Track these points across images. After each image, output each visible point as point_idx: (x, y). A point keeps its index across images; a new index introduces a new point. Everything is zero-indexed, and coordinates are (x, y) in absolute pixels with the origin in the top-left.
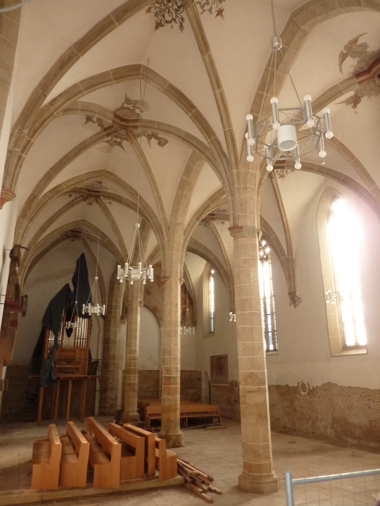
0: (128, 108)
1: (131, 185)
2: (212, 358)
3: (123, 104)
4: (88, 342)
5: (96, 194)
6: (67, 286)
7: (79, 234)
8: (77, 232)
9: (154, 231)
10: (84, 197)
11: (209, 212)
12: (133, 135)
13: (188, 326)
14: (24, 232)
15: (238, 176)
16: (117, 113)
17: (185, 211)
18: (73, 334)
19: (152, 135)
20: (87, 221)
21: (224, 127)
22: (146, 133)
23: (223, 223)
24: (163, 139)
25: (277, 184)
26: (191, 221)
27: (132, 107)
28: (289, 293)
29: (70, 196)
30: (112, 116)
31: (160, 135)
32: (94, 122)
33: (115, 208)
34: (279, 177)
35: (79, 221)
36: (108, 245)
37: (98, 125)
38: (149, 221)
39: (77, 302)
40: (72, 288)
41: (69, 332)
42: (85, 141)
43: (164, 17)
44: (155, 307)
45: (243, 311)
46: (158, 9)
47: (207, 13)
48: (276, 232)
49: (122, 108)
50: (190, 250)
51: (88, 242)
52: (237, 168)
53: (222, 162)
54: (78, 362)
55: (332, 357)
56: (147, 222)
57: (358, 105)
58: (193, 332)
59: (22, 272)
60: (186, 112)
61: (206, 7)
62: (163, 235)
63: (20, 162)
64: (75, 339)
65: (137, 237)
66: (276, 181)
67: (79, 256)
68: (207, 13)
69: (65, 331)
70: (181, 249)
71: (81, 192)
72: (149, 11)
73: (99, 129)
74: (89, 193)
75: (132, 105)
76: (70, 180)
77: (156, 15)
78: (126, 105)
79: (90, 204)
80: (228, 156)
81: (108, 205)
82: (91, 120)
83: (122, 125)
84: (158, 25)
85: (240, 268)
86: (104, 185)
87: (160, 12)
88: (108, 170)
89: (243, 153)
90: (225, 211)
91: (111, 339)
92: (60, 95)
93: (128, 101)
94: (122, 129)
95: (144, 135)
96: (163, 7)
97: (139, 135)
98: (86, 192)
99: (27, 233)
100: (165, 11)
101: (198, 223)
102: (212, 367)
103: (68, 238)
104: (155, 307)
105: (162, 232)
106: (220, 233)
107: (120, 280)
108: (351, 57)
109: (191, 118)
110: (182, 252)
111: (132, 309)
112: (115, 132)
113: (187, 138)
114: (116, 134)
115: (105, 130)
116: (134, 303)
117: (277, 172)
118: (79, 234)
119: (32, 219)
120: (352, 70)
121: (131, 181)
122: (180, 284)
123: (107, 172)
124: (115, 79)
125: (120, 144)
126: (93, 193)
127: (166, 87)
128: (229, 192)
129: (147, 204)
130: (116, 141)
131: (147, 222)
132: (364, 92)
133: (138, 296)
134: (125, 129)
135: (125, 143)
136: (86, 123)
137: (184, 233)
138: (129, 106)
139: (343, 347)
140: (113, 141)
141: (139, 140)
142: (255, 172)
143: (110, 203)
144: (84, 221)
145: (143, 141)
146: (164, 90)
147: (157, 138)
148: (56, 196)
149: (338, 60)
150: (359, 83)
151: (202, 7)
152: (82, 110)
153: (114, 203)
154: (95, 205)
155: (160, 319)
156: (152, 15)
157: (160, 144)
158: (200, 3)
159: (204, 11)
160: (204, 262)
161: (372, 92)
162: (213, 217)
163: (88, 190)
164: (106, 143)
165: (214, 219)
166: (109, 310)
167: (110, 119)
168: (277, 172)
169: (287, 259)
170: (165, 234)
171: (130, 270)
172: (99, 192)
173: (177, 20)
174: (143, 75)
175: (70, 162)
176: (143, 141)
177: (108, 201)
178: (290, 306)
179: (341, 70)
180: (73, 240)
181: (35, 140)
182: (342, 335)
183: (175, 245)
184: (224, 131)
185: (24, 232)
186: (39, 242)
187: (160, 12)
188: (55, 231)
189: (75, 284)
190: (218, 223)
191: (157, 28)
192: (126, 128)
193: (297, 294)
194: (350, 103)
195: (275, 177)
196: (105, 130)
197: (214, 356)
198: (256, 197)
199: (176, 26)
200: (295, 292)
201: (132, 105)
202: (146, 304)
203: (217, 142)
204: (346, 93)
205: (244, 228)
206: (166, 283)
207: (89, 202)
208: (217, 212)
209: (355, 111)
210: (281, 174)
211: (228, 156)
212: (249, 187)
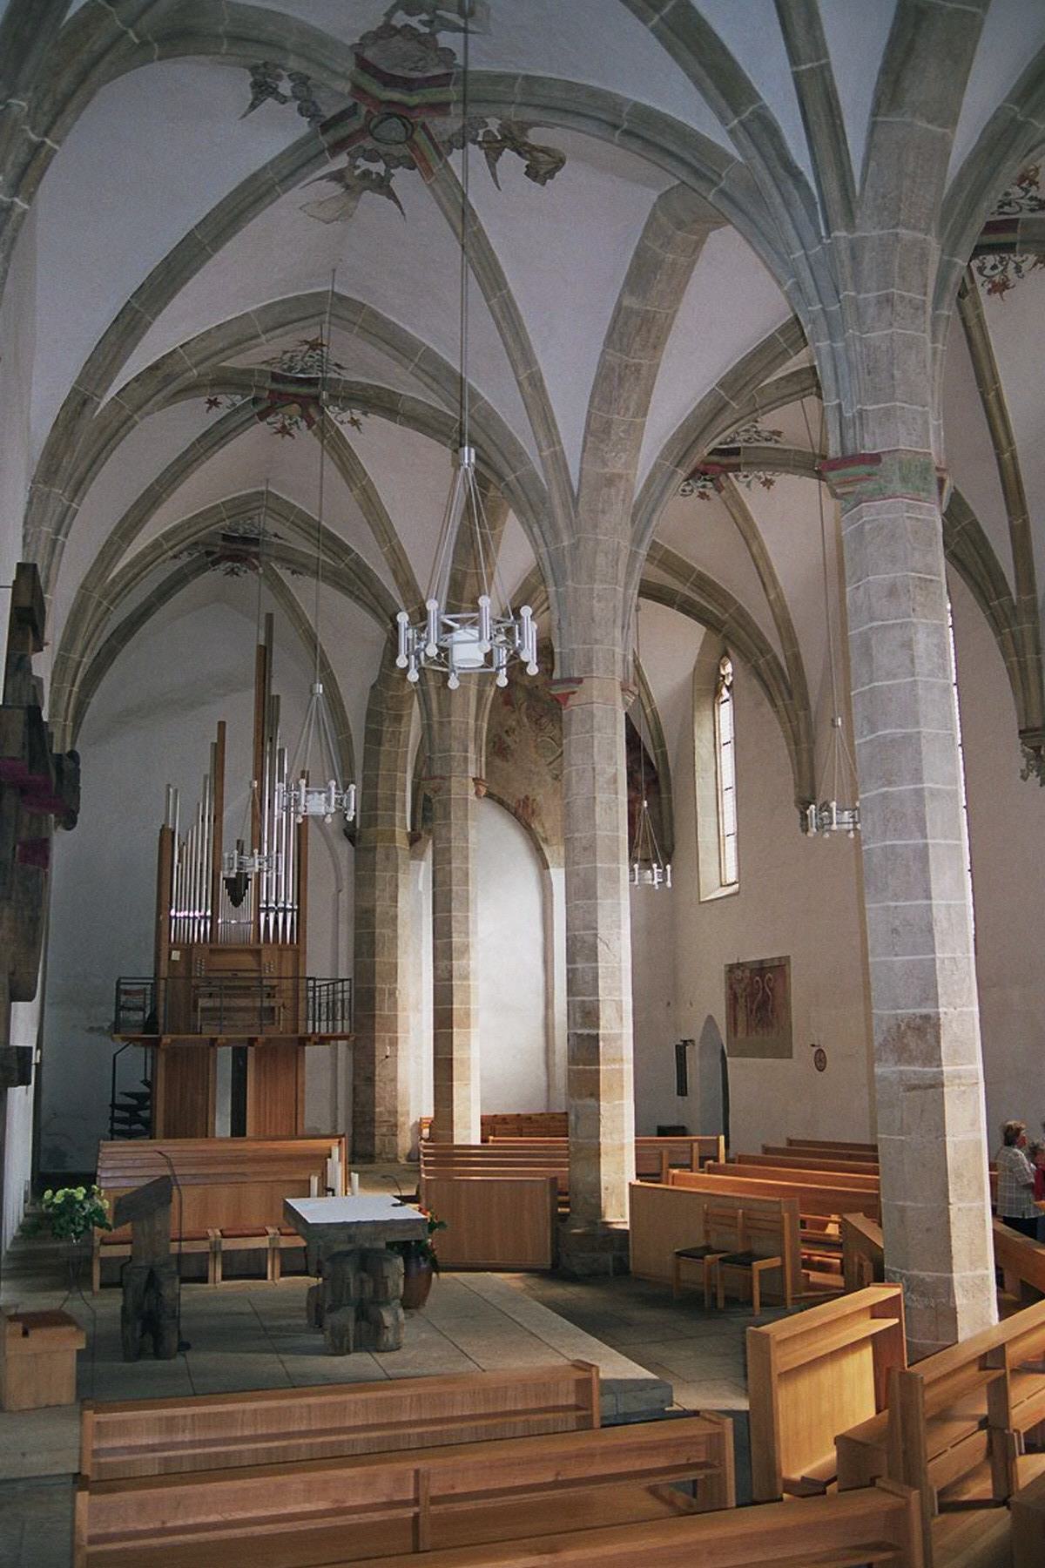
2: (731, 969)
3: (389, 15)
4: (300, 923)
7: (254, 549)
8: (246, 540)
9: (520, 513)
10: (262, 407)
11: (714, 444)
12: (431, 138)
13: (646, 864)
14: (57, 532)
15: (853, 258)
16: (369, 54)
17: (635, 431)
19: (505, 137)
21: (794, 58)
22: (481, 132)
23: (768, 483)
24: (544, 150)
25: (980, 317)
26: (657, 466)
27: (423, 23)
28: (1021, 732)
29: (213, 403)
30: (350, 65)
31: (535, 137)
32: (283, 100)
33: (373, 439)
34: (990, 291)
36: (354, 580)
37: (300, 110)
38: (501, 478)
42: (254, 177)
44: (527, 798)
45: (890, 783)
49: (387, 31)
50: (649, 591)
51: (285, 574)
52: (851, 225)
53: (787, 204)
54: (273, 987)
56: (494, 488)
58: (665, 880)
59: (67, 685)
62: (553, 525)
64: (259, 910)
65: (468, 506)
66: (977, 305)
69: (222, 883)
70: (622, 576)
71: (249, 387)
73: (303, 127)
74: (280, 387)
75: (424, 17)
78: (400, 19)
79: (284, 431)
80: (813, 185)
81: (347, 431)
82: (274, 92)
83: (391, 103)
85: (872, 619)
86: (334, 355)
89: (873, 164)
90: (779, 434)
91: (378, 909)
94: (390, 115)
95: (474, 142)
98: (269, 384)
99: (66, 536)
101: (682, 473)
102: (733, 1000)
103: (215, 563)
104: (527, 798)
105: (551, 515)
107: (407, 669)
110: (626, 588)
111: (446, 806)
112: (366, 131)
113: (644, 132)
114: (368, 143)
115: (326, 127)
116: (455, 785)
117: (981, 270)
118: (254, 549)
119: (80, 483)
121: (433, 330)
122: (626, 703)
125: (382, 186)
126: (293, 389)
128: (822, 321)
129: (490, 414)
130: (366, 174)
131: (494, 488)
133: (466, 758)
134: (399, 117)
135: (402, 179)
136: (253, 106)
137: (634, 516)
138: (414, 22)
140: (357, 172)
141: (455, 159)
142: (921, 236)
143: (354, 422)
144: (263, 500)
147: (521, 149)
148: (159, 397)
152: (237, 39)
153: (373, 422)
154: (305, 436)
157: (532, 173)
160: (697, 631)
162: (733, 460)
163: (275, 378)
164: (333, 184)
165: (736, 468)
166: (369, 803)
167: (343, 76)
168: (981, 270)
169: (1014, 608)
170: (561, 521)
171: (449, 630)
175: (204, 262)
176: (468, 163)
177: (346, 416)
178: (1024, 778)
180: (232, 572)
181: (58, 142)
183: (601, 560)
184: (797, 77)
185: (57, 532)
186: (113, 580)
188: (166, 536)
190: (748, 485)
195: (975, 289)
196: (326, 127)
197: (739, 965)
198: (928, 336)
201: (424, 17)
202: (495, 791)
203: (763, 130)
205: (884, 459)
206: (573, 700)
207: (278, 425)
210: (997, 279)
211: (813, 185)
212: (902, 297)
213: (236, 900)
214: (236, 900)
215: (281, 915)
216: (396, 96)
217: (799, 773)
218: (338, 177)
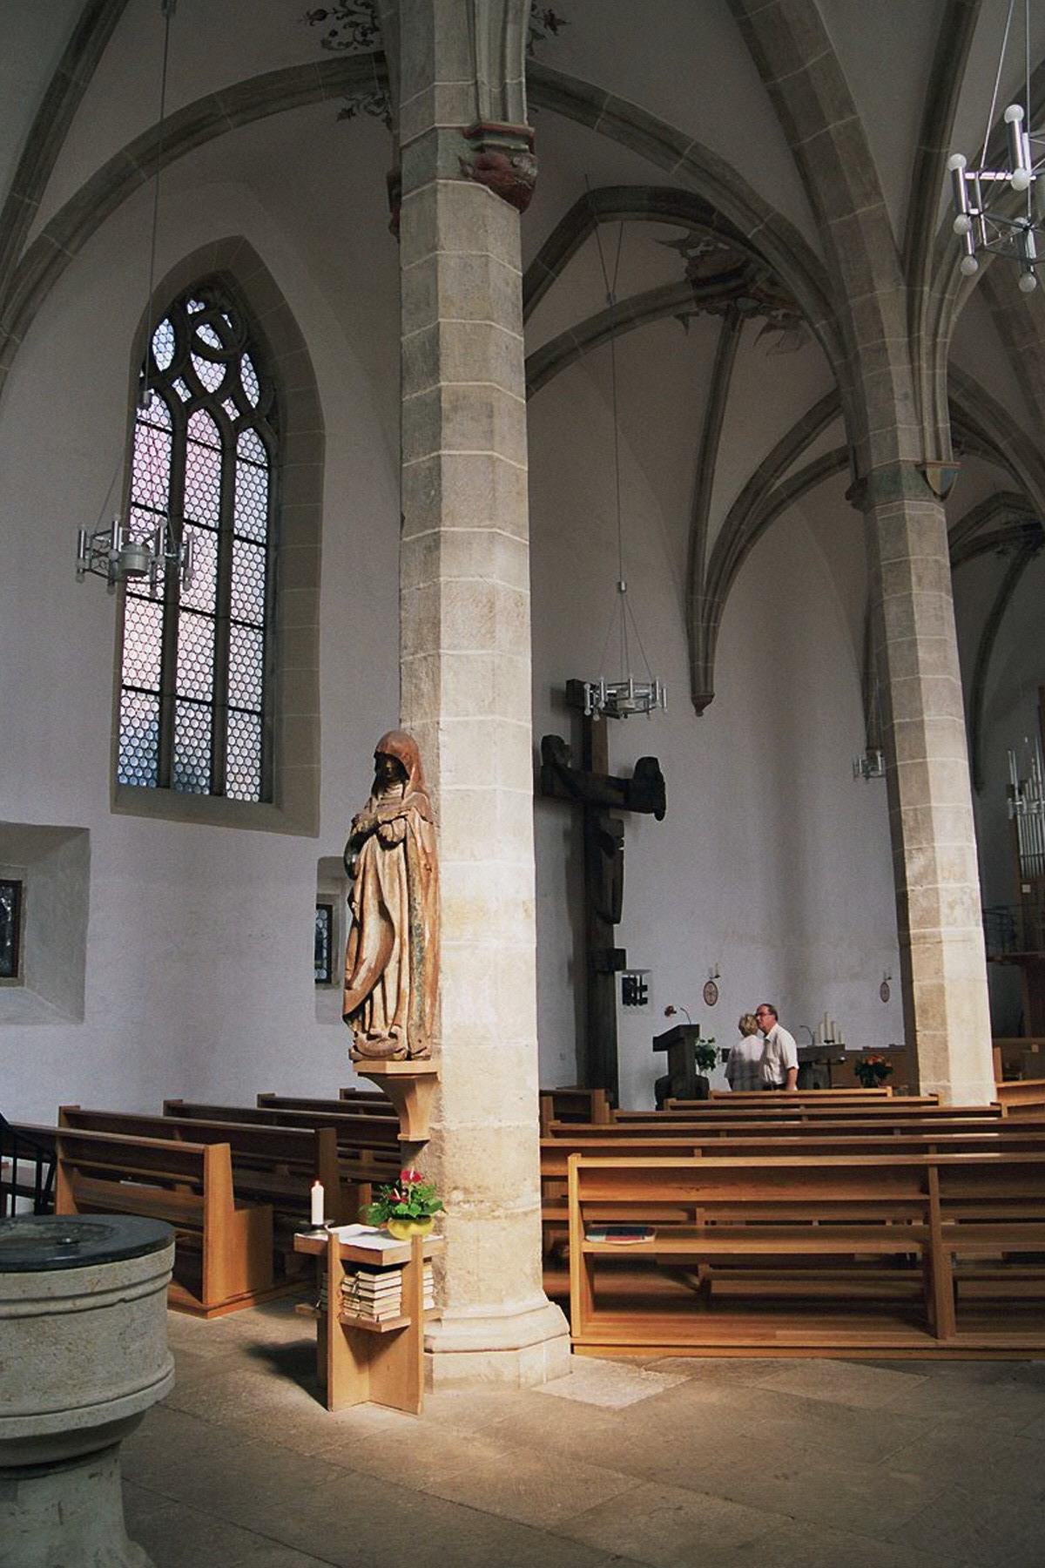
16: (703, 272)
30: (691, 293)
49: (694, 263)
83: (734, 290)
146: (644, 215)
216: (733, 284)
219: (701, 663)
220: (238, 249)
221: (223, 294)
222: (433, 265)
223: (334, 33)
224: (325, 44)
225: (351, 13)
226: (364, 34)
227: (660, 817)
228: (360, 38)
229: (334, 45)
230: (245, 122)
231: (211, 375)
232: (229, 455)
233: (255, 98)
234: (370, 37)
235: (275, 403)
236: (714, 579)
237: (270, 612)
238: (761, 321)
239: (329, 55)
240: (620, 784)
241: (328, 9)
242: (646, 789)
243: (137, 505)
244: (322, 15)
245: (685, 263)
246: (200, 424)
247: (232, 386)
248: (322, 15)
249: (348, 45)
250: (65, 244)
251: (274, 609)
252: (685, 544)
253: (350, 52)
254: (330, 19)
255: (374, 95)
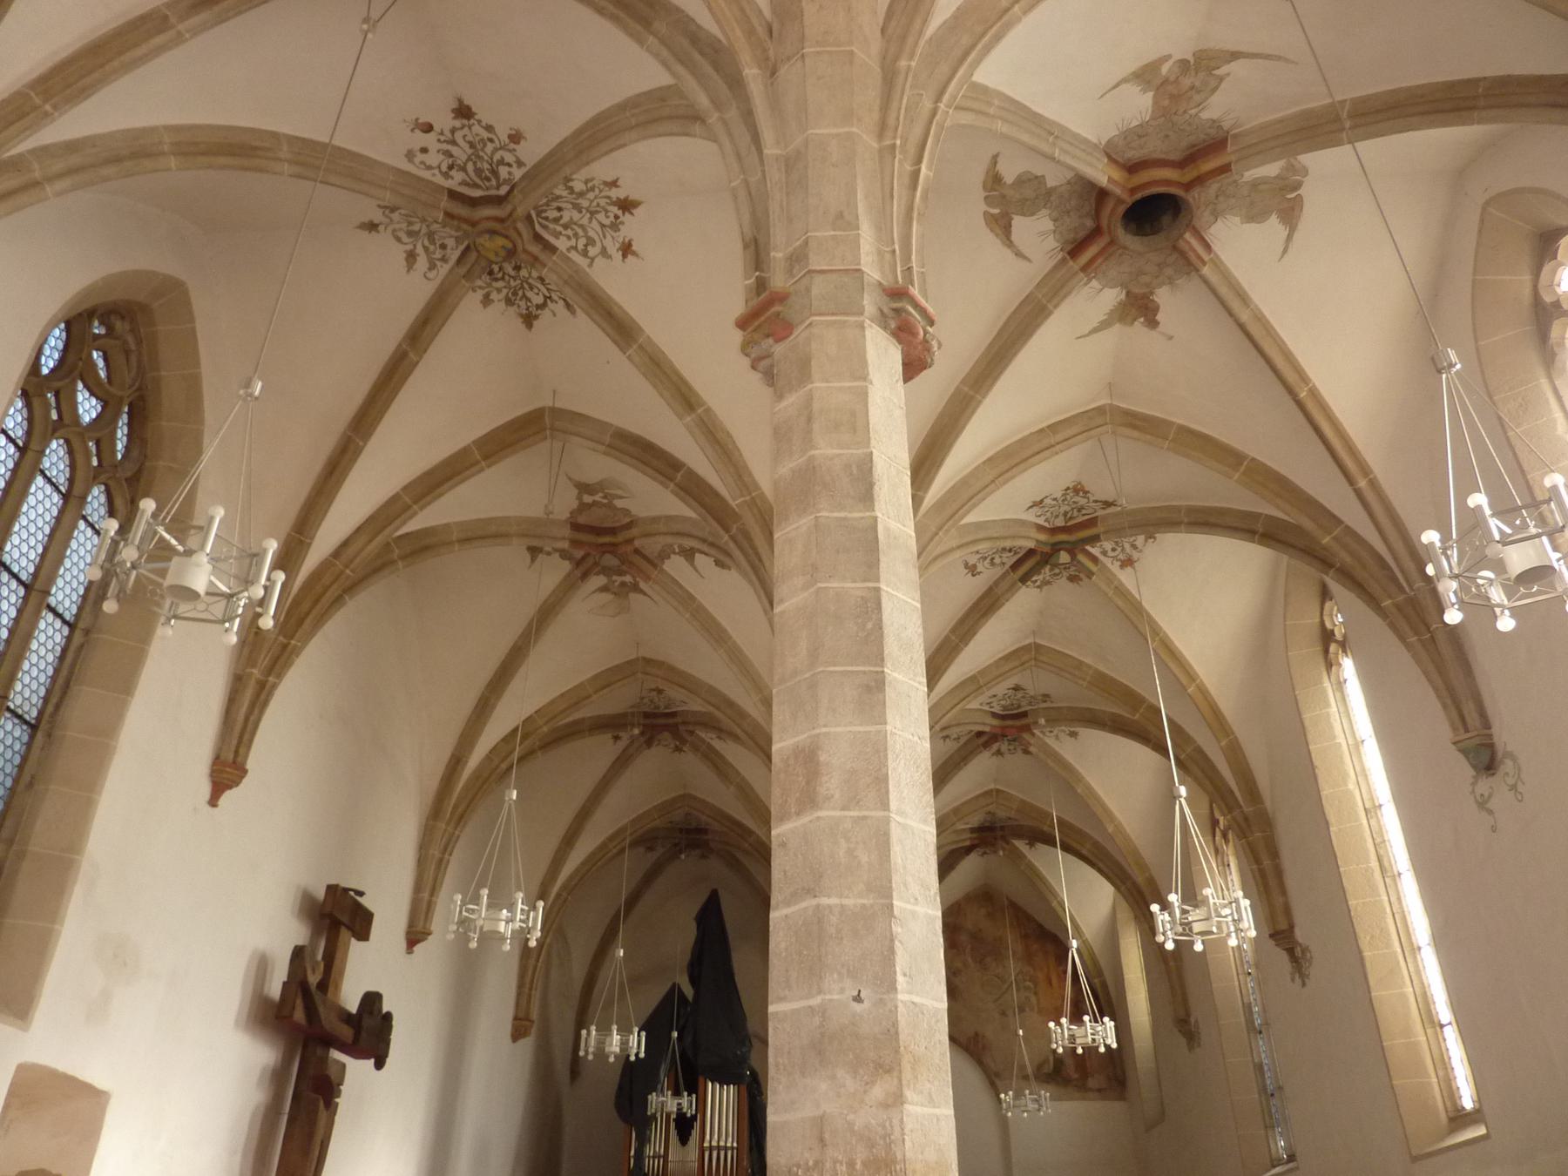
0: (595, 503)
1: (712, 682)
5: (671, 721)
6: (675, 990)
16: (582, 520)
18: (695, 1133)
20: (695, 798)
27: (1501, 532)
29: (616, 738)
30: (567, 532)
34: (1122, 567)
35: (674, 800)
39: (675, 1034)
40: (689, 992)
41: (684, 1126)
43: (529, 300)
44: (976, 1034)
46: (505, 291)
47: (599, 261)
48: (1192, 733)
49: (583, 507)
55: (1415, 1159)
57: (1158, 317)
60: (662, 483)
61: (592, 251)
63: (263, 697)
64: (702, 1150)
67: (702, 898)
68: (599, 261)
72: (486, 301)
73: (566, 566)
76: (552, 702)
77: (509, 302)
83: (602, 545)
84: (529, 320)
87: (515, 294)
88: (648, 655)
92: (358, 530)
93: (583, 488)
96: (513, 283)
97: (664, 555)
100: (522, 287)
104: (976, 1034)
106: (1077, 767)
108: (1024, 215)
109: (677, 495)
112: (596, 564)
120: (1052, 243)
123: (648, 661)
124: (486, 458)
125: (635, 588)
127: (608, 439)
130: (623, 584)
132: (1146, 279)
136: (533, 560)
139: (1452, 1120)
145: (676, 566)
146: (603, 448)
149: (991, 236)
150: (1084, 269)
151: (585, 253)
155: (997, 1075)
156: (498, 306)
158: (575, 248)
159: (593, 259)
161: (1169, 271)
172: (673, 715)
173: (554, 297)
174: (552, 429)
179: (1019, 254)
182: (1441, 1073)
187: (515, 294)
189: (694, 981)
191: (529, 325)
192: (612, 548)
193: (1299, 934)
194: (1135, 319)
199: (559, 307)
200: (1292, 927)
204: (1056, 306)
208: (1030, 704)
209: (1163, 334)
210: (1121, 557)
213: (684, 1139)
214: (684, 1139)
215: (715, 1154)
216: (606, 539)
217: (418, 887)
218: (604, 589)
219: (426, 895)
220: (173, 292)
221: (132, 331)
222: (863, 396)
223: (424, 150)
224: (410, 155)
225: (454, 143)
226: (451, 167)
227: (379, 1065)
228: (444, 168)
229: (417, 160)
230: (299, 176)
231: (88, 408)
232: (72, 500)
233: (318, 161)
234: (453, 173)
235: (140, 471)
236: (460, 810)
237: (50, 708)
238: (601, 580)
239: (405, 166)
240: (347, 1018)
241: (437, 128)
242: (370, 1032)
243: (84, 518)
244: (428, 128)
245: (575, 505)
246: (55, 458)
247: (105, 421)
248: (428, 128)
249: (429, 168)
250: (50, 179)
251: (58, 707)
252: (440, 770)
253: (426, 175)
254: (432, 136)
255: (410, 224)
